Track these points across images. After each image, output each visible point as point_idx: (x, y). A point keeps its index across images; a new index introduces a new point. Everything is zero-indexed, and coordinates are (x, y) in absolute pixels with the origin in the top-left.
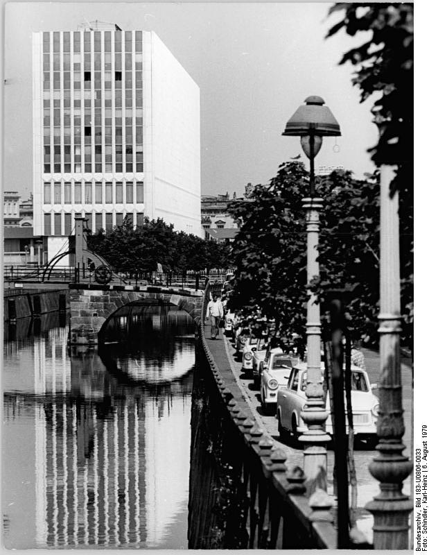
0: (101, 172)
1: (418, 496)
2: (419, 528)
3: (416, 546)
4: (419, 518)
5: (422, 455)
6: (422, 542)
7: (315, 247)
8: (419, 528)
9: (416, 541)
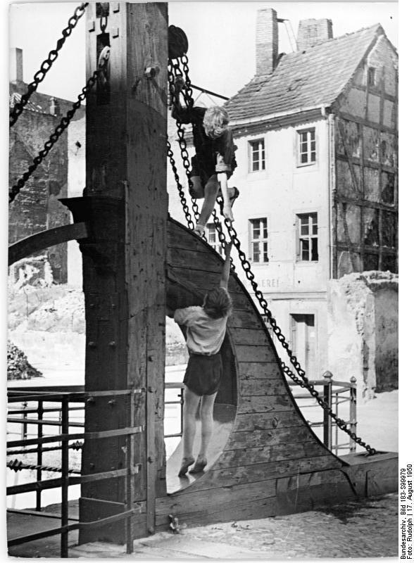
0: (10, 401)
1: (403, 503)
2: (404, 536)
3: (400, 554)
4: (404, 525)
5: (407, 495)
6: (407, 550)
7: (373, 388)
8: (404, 536)
9: (400, 549)
